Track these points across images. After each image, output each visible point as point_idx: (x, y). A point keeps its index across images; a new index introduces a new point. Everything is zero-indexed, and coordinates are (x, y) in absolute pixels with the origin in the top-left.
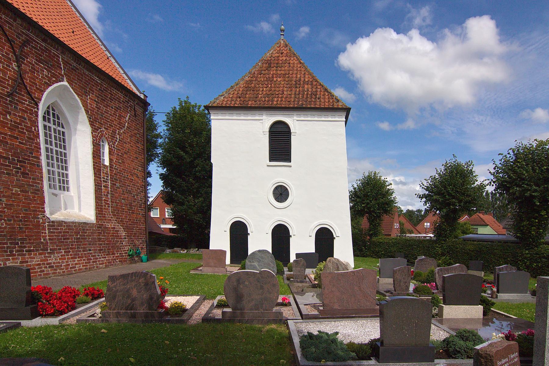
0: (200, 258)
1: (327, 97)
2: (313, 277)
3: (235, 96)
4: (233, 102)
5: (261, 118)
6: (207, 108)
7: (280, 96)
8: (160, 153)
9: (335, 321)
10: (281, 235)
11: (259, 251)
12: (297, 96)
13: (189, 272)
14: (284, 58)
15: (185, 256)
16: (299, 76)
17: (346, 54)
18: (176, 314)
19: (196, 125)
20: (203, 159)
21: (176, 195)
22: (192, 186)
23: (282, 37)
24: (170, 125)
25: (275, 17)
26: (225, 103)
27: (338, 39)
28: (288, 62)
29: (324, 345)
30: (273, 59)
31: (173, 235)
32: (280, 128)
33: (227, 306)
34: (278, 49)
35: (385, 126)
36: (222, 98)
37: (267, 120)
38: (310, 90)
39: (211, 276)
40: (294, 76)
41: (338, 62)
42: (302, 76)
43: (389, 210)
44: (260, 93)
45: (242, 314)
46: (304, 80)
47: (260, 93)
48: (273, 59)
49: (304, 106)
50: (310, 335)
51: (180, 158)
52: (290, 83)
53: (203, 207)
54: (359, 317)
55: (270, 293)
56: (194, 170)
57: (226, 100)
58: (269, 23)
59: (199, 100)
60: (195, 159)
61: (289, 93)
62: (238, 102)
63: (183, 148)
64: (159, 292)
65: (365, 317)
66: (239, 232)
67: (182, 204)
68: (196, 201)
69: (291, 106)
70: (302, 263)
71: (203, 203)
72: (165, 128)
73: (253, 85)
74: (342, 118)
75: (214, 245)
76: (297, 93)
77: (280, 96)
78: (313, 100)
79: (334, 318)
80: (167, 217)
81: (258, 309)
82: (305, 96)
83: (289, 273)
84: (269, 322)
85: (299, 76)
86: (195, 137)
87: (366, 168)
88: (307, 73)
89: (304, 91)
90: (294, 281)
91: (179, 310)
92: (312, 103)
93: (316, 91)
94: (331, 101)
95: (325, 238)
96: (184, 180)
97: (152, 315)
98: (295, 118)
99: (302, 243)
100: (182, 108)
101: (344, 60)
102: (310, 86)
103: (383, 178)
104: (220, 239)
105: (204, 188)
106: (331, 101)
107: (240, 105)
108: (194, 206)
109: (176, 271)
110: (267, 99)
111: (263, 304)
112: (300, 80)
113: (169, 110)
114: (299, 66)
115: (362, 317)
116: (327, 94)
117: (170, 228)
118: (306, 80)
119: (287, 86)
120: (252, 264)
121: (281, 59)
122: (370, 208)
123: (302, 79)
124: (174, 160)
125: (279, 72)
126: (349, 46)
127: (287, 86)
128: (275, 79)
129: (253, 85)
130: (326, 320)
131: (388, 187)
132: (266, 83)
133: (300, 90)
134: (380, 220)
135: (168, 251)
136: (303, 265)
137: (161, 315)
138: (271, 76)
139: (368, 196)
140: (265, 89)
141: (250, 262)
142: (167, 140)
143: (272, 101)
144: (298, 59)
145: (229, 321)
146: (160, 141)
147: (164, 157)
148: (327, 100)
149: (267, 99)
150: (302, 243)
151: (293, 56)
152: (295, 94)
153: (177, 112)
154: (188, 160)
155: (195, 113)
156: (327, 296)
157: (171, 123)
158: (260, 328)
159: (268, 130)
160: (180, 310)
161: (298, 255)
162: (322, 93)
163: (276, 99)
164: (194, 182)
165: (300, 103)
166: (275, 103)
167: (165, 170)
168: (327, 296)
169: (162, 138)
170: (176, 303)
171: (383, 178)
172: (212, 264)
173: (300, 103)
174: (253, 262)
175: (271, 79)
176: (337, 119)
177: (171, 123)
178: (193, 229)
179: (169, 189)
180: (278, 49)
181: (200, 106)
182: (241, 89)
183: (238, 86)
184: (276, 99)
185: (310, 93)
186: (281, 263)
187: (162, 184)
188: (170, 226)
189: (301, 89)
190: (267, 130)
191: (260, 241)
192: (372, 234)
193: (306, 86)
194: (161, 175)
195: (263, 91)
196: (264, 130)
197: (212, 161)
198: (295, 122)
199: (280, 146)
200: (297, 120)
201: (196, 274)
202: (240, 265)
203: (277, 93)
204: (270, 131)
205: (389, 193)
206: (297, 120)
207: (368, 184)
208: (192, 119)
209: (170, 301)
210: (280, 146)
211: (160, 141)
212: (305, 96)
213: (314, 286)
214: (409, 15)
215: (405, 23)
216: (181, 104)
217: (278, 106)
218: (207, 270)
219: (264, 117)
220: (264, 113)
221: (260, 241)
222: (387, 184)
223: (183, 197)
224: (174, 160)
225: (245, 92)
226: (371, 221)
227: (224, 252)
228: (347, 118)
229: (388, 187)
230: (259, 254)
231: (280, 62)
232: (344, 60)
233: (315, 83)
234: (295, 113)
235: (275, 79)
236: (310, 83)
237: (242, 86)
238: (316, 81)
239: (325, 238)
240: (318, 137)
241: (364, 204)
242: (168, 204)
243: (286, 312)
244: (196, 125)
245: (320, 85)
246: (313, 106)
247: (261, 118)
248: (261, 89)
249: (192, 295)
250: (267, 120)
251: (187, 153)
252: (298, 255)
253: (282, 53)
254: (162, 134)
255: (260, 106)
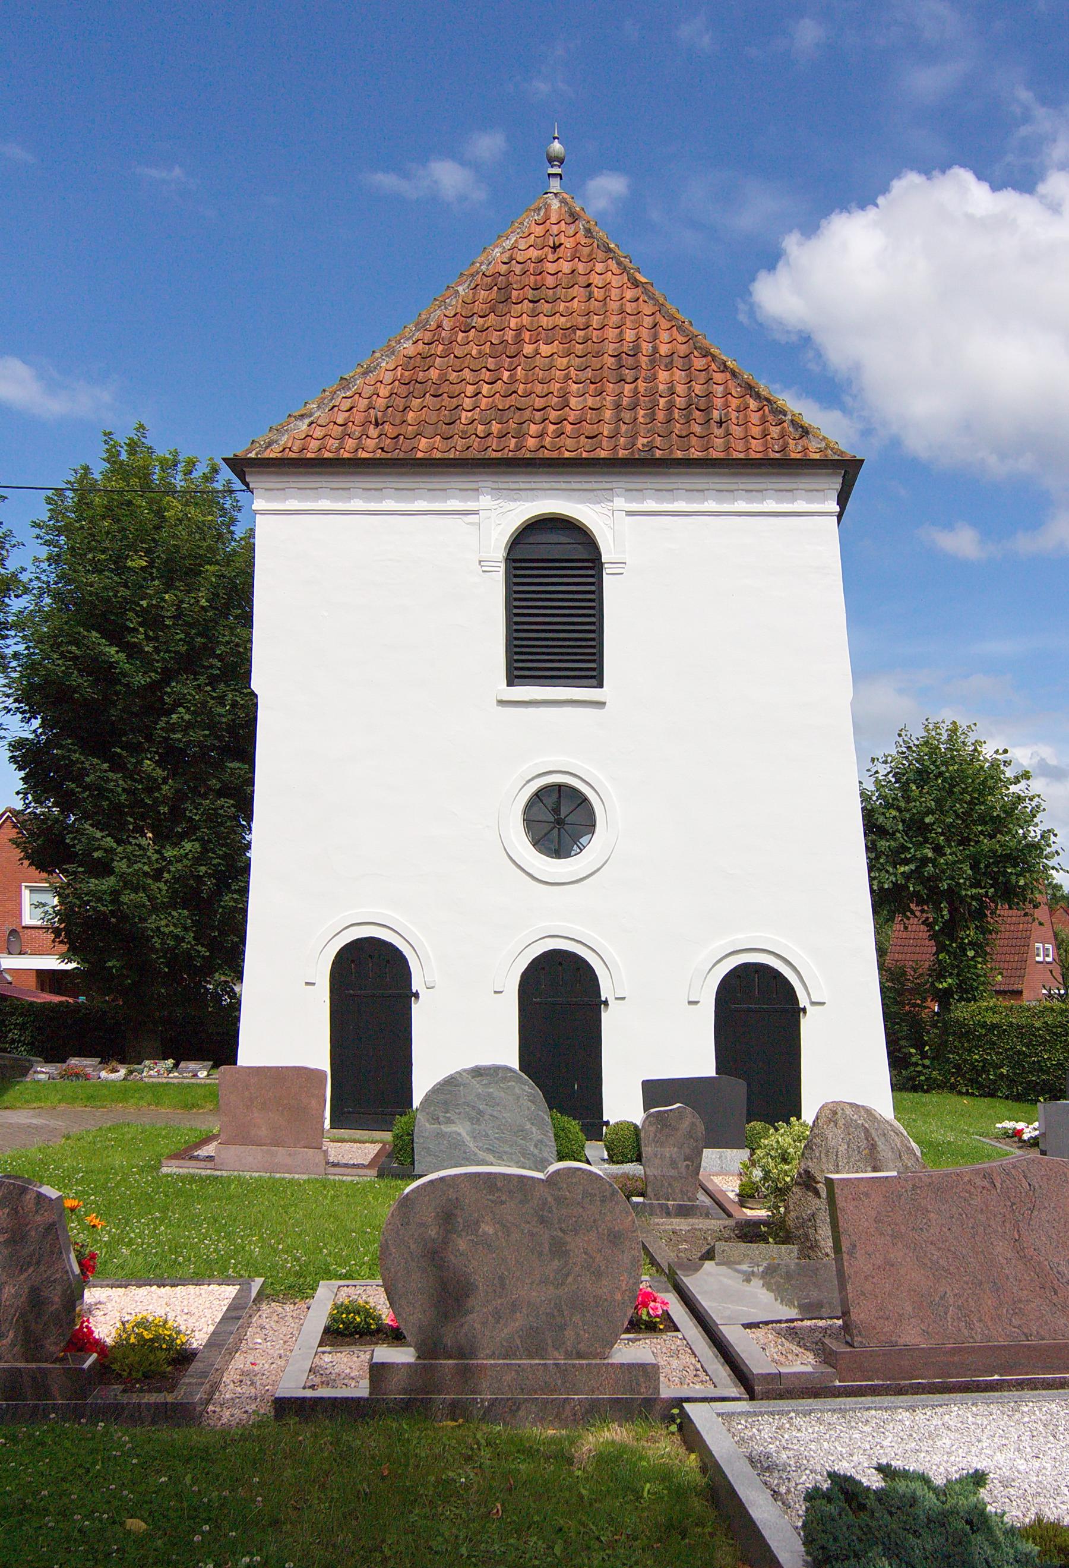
0: (189, 1100)
1: (755, 418)
2: (729, 1187)
3: (359, 417)
4: (350, 443)
5: (470, 505)
6: (240, 466)
7: (553, 415)
8: (16, 656)
9: (912, 1409)
10: (561, 1002)
11: (478, 1072)
12: (627, 416)
13: (156, 1168)
14: (566, 267)
15: (123, 1092)
16: (629, 335)
17: (782, 273)
18: (146, 1376)
19: (174, 536)
20: (202, 679)
21: (80, 832)
22: (149, 791)
23: (555, 185)
24: (63, 540)
25: (488, 145)
26: (314, 445)
27: (757, 208)
28: (582, 280)
29: (930, 1543)
30: (518, 269)
31: (56, 999)
32: (555, 546)
33: (395, 1336)
34: (539, 230)
35: (962, 542)
36: (303, 426)
37: (500, 514)
38: (680, 389)
39: (259, 1186)
40: (611, 334)
41: (752, 310)
42: (645, 333)
43: (1024, 888)
44: (468, 403)
45: (466, 1374)
46: (655, 350)
47: (468, 403)
48: (518, 269)
49: (658, 454)
50: (845, 1489)
51: (103, 672)
52: (595, 363)
53: (199, 879)
54: (1020, 1385)
55: (599, 1275)
56: (161, 724)
57: (319, 433)
58: (463, 163)
59: (192, 439)
60: (168, 676)
61: (590, 402)
62: (370, 444)
63: (116, 635)
64: (77, 1270)
65: (1048, 1385)
66: (371, 986)
67: (103, 869)
68: (169, 853)
69: (603, 454)
70: (685, 1125)
71: (198, 861)
72: (44, 552)
73: (434, 374)
74: (823, 501)
75: (254, 1049)
76: (625, 401)
77: (553, 415)
78: (697, 429)
79: (900, 1391)
80: (27, 920)
81: (537, 1350)
82: (661, 416)
83: (616, 1169)
84: (594, 1413)
85: (629, 335)
86: (169, 586)
87: (914, 714)
88: (664, 324)
89: (653, 393)
90: (651, 1210)
91: (162, 1355)
92: (694, 440)
93: (709, 395)
94: (775, 431)
95: (758, 1011)
96: (117, 765)
97: (40, 1384)
98: (620, 503)
99: (656, 1037)
100: (117, 468)
101: (778, 297)
102: (679, 375)
103: (988, 751)
104: (284, 1020)
105: (204, 796)
106: (775, 431)
107: (379, 454)
108: (157, 875)
109: (95, 1164)
110: (495, 427)
111: (562, 1328)
112: (635, 353)
113: (62, 476)
114: (629, 294)
115: (1033, 1385)
116: (753, 404)
117: (40, 973)
118: (664, 349)
119: (583, 376)
120: (447, 1129)
121: (551, 268)
122: (935, 878)
123: (646, 348)
124: (76, 679)
125: (544, 321)
126: (792, 243)
127: (583, 376)
128: (528, 349)
129: (434, 374)
130: (867, 1400)
131: (1013, 789)
132: (491, 363)
133: (636, 392)
134: (983, 930)
135: (43, 1071)
136: (690, 1135)
137: (83, 1383)
138: (509, 335)
139: (924, 829)
140: (485, 389)
141: (436, 1120)
142: (48, 600)
143: (520, 436)
144: (625, 269)
145: (406, 1407)
146: (17, 604)
147: (31, 667)
148: (756, 431)
149: (495, 427)
150: (656, 1037)
151: (600, 255)
152: (618, 406)
153: (93, 488)
154: (140, 680)
155: (172, 491)
156: (868, 1286)
157: (66, 530)
158: (552, 1440)
159: (500, 554)
160: (159, 1360)
161: (656, 1092)
162: (734, 403)
163: (533, 429)
164: (160, 773)
165: (641, 441)
166: (531, 443)
167: (36, 723)
168: (868, 1286)
169: (27, 591)
170: (143, 1324)
171: (988, 751)
172: (263, 1132)
173: (641, 441)
174: (449, 1121)
175: (512, 350)
176: (801, 506)
177: (66, 530)
178: (154, 980)
179: (50, 808)
180: (539, 230)
181: (191, 464)
182: (384, 391)
183: (371, 378)
184: (533, 429)
185: (680, 402)
186: (574, 1126)
187: (20, 785)
188: (52, 963)
189: (642, 386)
190: (499, 553)
191: (463, 1029)
192: (948, 993)
193: (663, 376)
194: (18, 745)
195: (477, 400)
196: (484, 556)
197: (257, 684)
198: (617, 521)
199: (554, 617)
200: (630, 513)
201: (193, 1179)
202: (388, 1136)
203: (539, 403)
204: (508, 560)
205: (1014, 814)
206: (630, 513)
207: (922, 776)
208: (159, 513)
209: (112, 1311)
210: (554, 617)
211: (17, 604)
212: (661, 416)
213: (750, 1233)
214: (1024, 131)
215: (1010, 158)
216: (112, 457)
217: (547, 454)
218: (237, 1162)
219: (485, 501)
220: (486, 482)
221: (463, 1029)
222: (1009, 773)
223: (110, 842)
224: (76, 679)
225: (400, 403)
226: (945, 935)
227: (320, 1073)
228: (843, 499)
229: (1013, 789)
230: (477, 1086)
231: (550, 281)
232: (778, 297)
233: (699, 363)
234: (619, 483)
235: (528, 349)
236: (678, 362)
237: (388, 377)
238: (706, 354)
239: (758, 1011)
240: (718, 583)
241: (906, 862)
242: (41, 866)
243: (675, 1362)
244: (174, 536)
245: (724, 368)
246: (695, 454)
247: (470, 505)
248: (470, 390)
249: (197, 1279)
250: (500, 514)
251: (132, 651)
252: (656, 1092)
253: (555, 248)
254: (24, 577)
255: (468, 455)
